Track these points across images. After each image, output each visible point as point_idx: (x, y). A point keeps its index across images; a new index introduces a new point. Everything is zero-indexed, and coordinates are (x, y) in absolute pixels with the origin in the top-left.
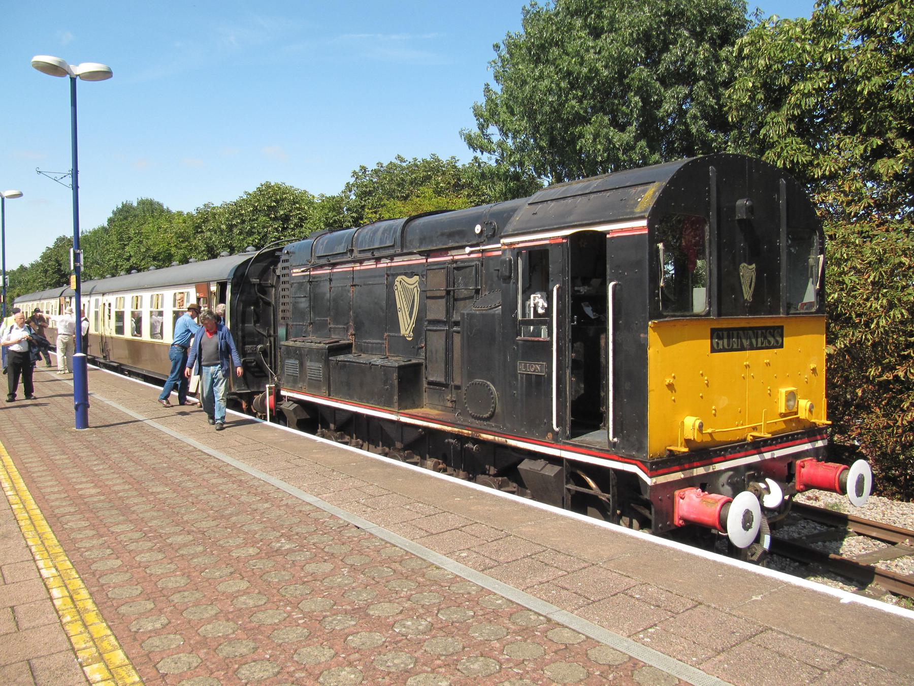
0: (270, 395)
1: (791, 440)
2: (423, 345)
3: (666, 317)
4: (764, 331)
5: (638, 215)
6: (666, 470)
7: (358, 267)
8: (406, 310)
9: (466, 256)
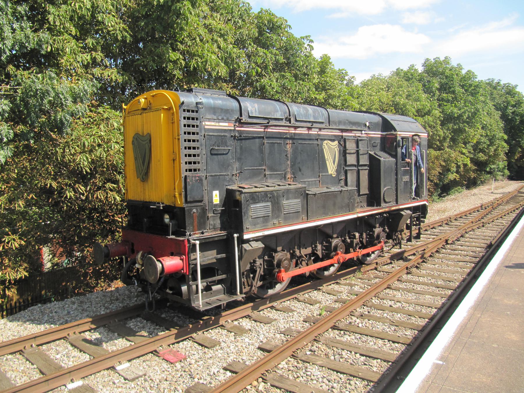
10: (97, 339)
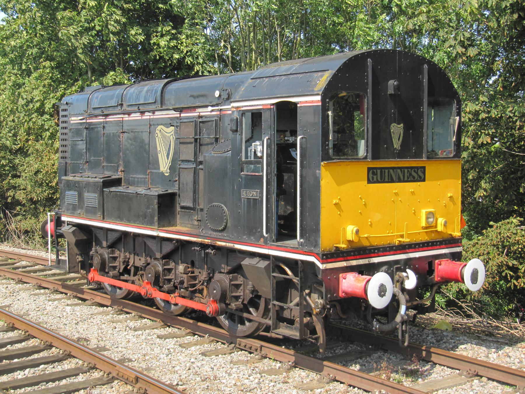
0: (51, 221)
1: (431, 246)
2: (177, 179)
3: (334, 159)
4: (410, 170)
5: (315, 93)
6: (333, 260)
7: (126, 118)
8: (165, 152)
9: (209, 113)
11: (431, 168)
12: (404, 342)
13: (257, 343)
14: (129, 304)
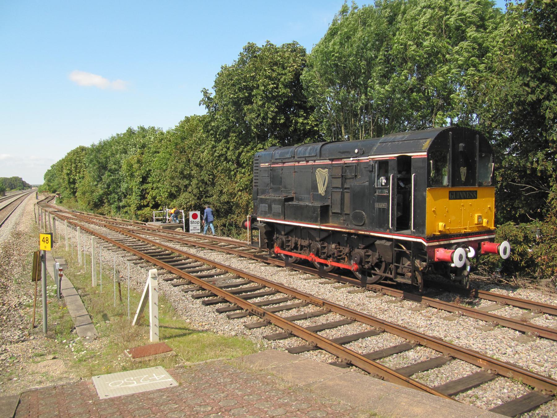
6: (432, 241)
7: (297, 164)
10: (162, 219)
11: (480, 192)
12: (466, 286)
13: (379, 287)
14: (297, 266)
